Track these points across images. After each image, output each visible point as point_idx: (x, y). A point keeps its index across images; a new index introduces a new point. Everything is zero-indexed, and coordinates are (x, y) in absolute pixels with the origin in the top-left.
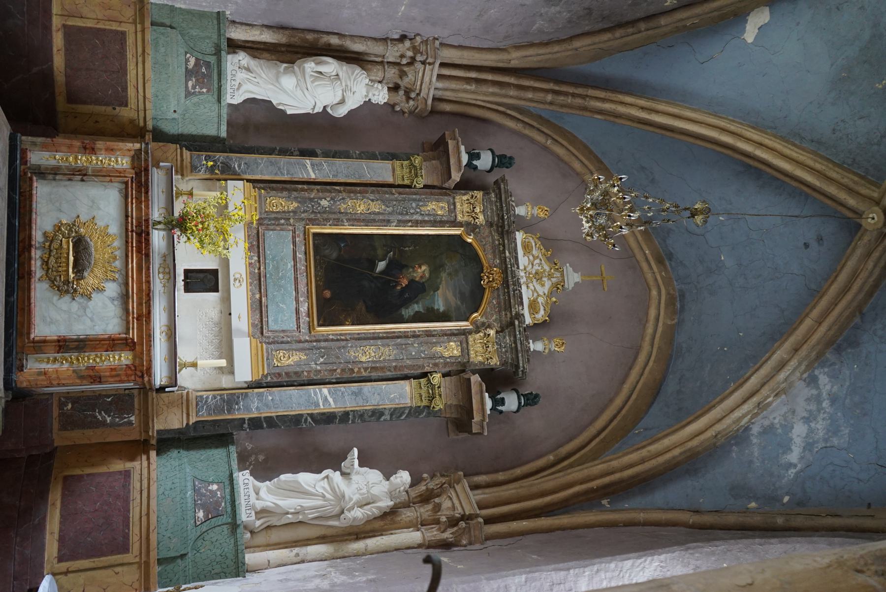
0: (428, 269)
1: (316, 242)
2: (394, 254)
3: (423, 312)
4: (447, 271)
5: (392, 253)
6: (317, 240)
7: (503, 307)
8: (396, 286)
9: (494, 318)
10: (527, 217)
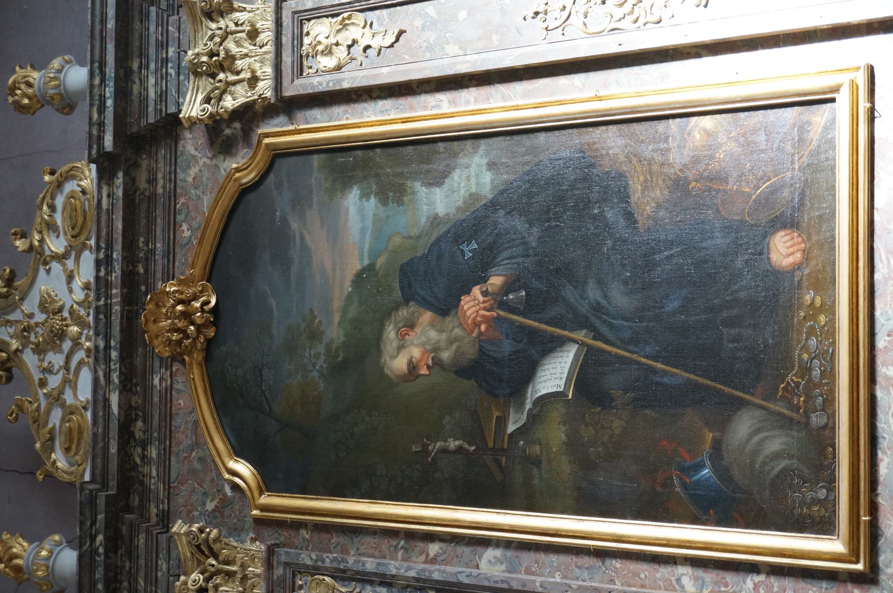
0: (386, 357)
1: (822, 494)
2: (502, 421)
3: (417, 185)
4: (321, 349)
5: (511, 428)
6: (816, 501)
7: (159, 211)
8: (508, 288)
9: (193, 171)
10: (58, 544)
